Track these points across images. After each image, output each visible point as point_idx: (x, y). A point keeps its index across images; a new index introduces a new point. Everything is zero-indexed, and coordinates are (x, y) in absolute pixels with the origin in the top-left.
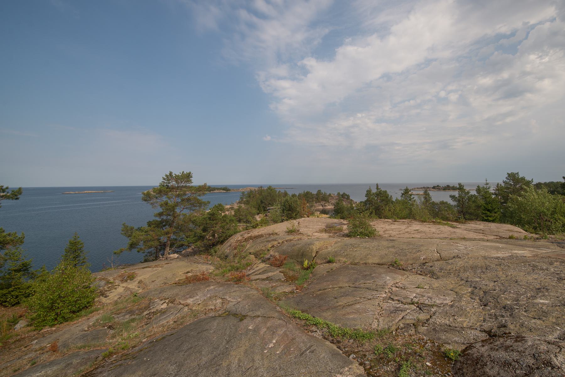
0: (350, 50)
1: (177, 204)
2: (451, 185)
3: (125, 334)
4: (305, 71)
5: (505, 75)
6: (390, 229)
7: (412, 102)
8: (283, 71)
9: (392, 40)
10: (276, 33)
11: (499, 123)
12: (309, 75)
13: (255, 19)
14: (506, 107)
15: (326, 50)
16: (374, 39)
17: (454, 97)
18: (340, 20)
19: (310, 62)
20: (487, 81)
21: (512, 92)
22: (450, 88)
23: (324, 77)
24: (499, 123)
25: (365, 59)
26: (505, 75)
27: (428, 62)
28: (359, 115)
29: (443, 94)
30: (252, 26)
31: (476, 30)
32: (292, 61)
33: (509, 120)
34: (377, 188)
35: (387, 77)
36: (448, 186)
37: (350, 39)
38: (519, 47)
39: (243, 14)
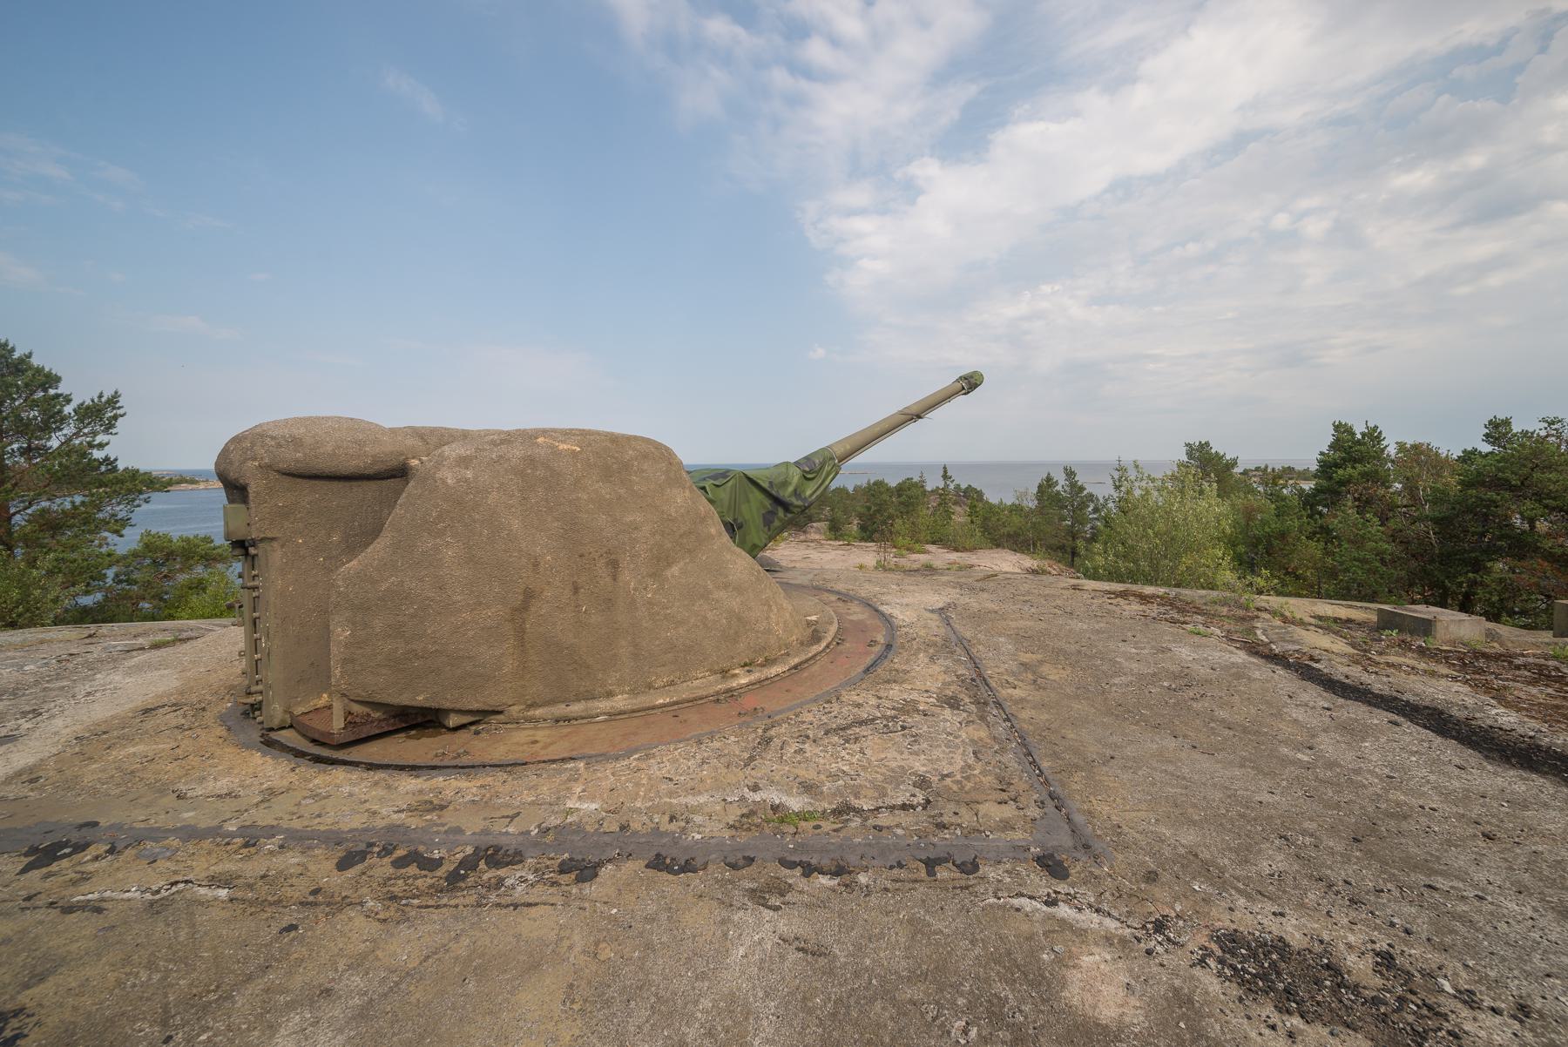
0: (1031, 134)
1: (1041, 662)
2: (1299, 468)
3: (68, 506)
4: (912, 190)
5: (1476, 160)
6: (805, 554)
7: (1193, 248)
8: (859, 195)
9: (1140, 96)
10: (846, 109)
11: (1463, 290)
12: (921, 200)
13: (804, 85)
14: (1483, 245)
15: (966, 138)
16: (1093, 101)
17: (1315, 228)
18: (1005, 68)
19: (928, 170)
20: (1419, 179)
21: (1495, 204)
22: (1304, 204)
23: (961, 202)
24: (1463, 290)
25: (1069, 148)
26: (1476, 160)
27: (1238, 142)
28: (1046, 289)
29: (1281, 221)
30: (796, 101)
31: (1383, 48)
32: (881, 168)
33: (1495, 280)
34: (945, 477)
35: (1124, 188)
36: (1291, 469)
37: (1027, 106)
38: (1519, 79)
39: (780, 77)
